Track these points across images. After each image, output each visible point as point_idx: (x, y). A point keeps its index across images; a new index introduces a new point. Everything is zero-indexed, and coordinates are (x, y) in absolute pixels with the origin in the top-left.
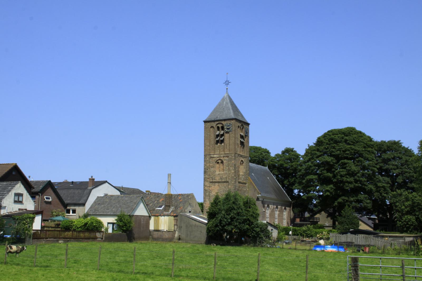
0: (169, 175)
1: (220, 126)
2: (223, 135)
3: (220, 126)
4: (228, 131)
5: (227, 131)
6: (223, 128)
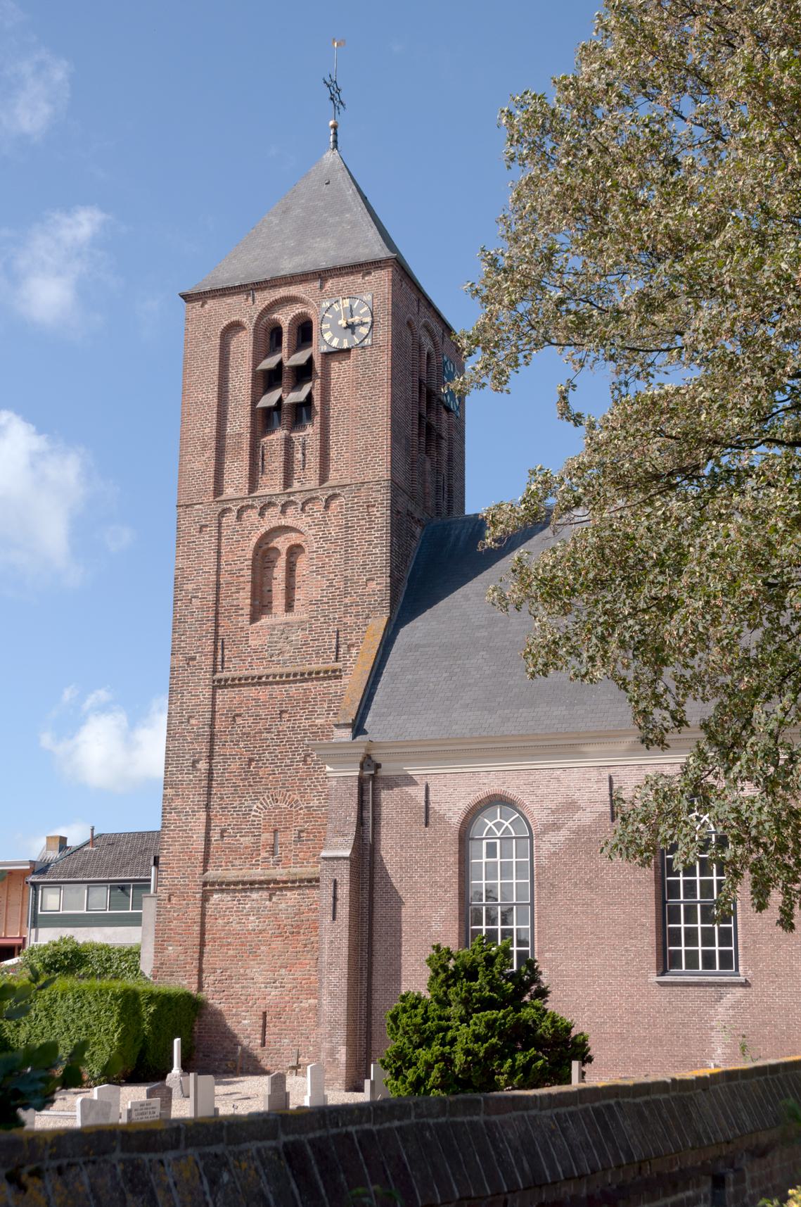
0: (187, 298)
2: (304, 373)
3: (285, 318)
4: (345, 346)
5: (335, 343)
6: (304, 332)
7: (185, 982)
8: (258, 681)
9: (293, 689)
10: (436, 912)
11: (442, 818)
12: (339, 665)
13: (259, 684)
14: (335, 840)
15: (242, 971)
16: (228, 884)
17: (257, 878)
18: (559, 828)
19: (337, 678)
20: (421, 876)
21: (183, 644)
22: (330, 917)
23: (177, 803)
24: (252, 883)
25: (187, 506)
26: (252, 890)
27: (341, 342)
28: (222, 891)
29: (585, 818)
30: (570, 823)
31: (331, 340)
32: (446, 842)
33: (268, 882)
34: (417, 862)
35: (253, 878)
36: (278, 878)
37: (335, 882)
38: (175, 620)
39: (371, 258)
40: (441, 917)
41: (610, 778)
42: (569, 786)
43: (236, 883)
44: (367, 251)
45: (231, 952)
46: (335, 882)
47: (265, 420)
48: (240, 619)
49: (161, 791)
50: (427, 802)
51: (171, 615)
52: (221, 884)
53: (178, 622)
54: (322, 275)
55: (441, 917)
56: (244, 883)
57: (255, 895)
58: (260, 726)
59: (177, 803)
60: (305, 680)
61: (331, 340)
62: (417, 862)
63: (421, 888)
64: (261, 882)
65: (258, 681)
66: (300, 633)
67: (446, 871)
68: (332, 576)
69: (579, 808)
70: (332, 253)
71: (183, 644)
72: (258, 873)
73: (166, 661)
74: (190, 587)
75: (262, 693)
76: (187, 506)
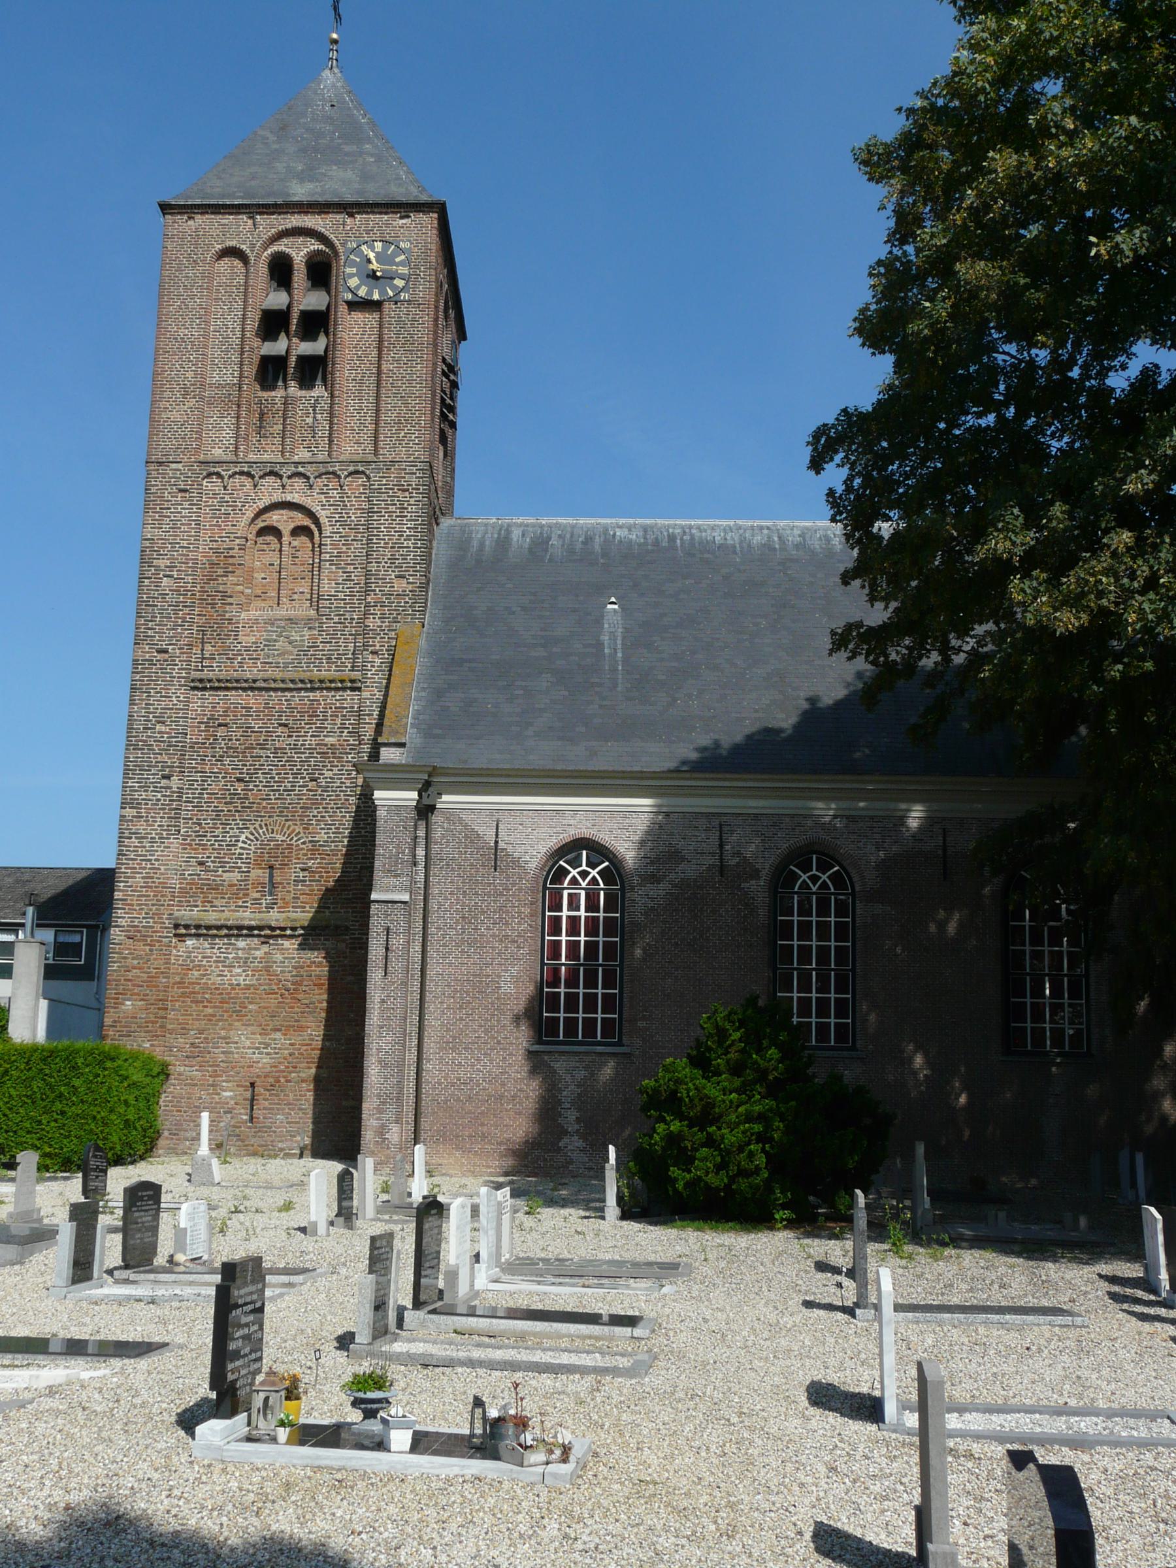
0: (165, 208)
1: (299, 252)
2: (316, 323)
3: (299, 252)
4: (376, 297)
5: (362, 292)
6: (321, 272)
7: (147, 1045)
8: (251, 687)
9: (297, 698)
10: (506, 971)
11: (516, 862)
12: (357, 675)
13: (252, 689)
14: (386, 880)
15: (223, 1033)
16: (208, 928)
17: (246, 923)
18: (658, 881)
19: (353, 689)
20: (488, 929)
21: (150, 633)
22: (381, 972)
23: (141, 827)
24: (240, 928)
25: (160, 463)
26: (238, 936)
27: (370, 293)
28: (198, 936)
29: (690, 870)
30: (672, 876)
31: (358, 287)
32: (520, 889)
33: (260, 928)
34: (483, 912)
35: (239, 923)
36: (273, 924)
37: (388, 929)
38: (140, 602)
39: (411, 199)
40: (512, 976)
41: (721, 825)
42: (672, 834)
43: (219, 928)
44: (402, 190)
45: (210, 1011)
46: (388, 929)
47: (271, 371)
48: (228, 608)
49: (117, 812)
50: (496, 842)
51: (136, 595)
52: (198, 927)
53: (143, 608)
54: (350, 208)
55: (512, 976)
56: (229, 928)
57: (241, 943)
58: (252, 740)
59: (141, 827)
60: (312, 689)
61: (358, 287)
62: (483, 912)
63: (488, 942)
64: (251, 928)
65: (251, 687)
66: (306, 633)
67: (519, 923)
68: (350, 568)
69: (683, 859)
70: (356, 186)
71: (150, 633)
72: (247, 917)
73: (125, 652)
74: (163, 563)
75: (252, 700)
76: (160, 463)
